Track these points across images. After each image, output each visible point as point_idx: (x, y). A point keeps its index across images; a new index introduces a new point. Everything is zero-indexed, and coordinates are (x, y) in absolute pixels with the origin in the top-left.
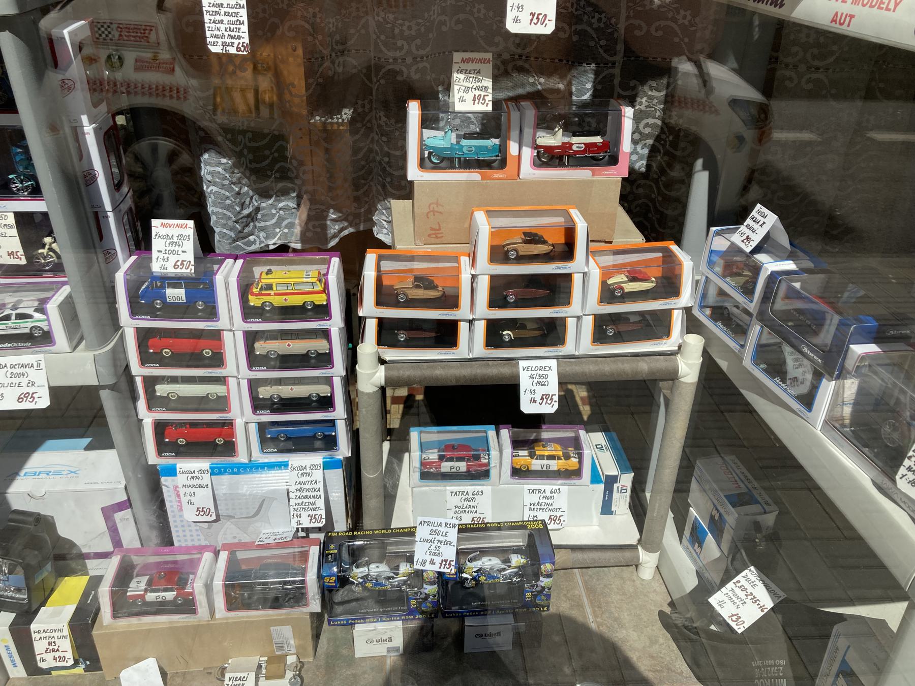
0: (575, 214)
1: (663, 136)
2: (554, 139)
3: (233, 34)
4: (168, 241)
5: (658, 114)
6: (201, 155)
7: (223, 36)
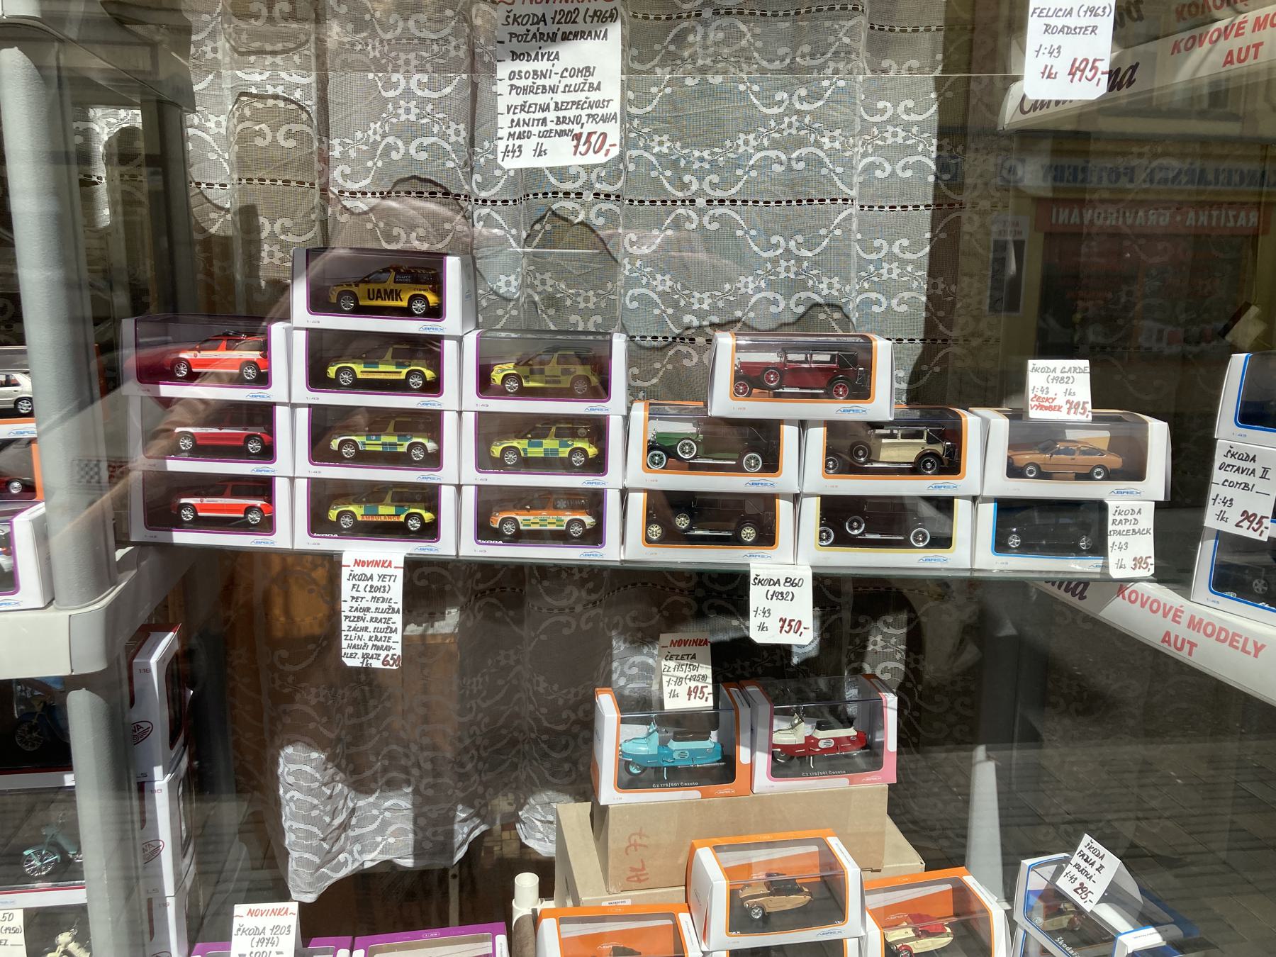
0: (835, 843)
1: (909, 685)
2: (790, 733)
3: (379, 644)
4: (257, 938)
5: (898, 656)
6: (282, 747)
7: (366, 646)
